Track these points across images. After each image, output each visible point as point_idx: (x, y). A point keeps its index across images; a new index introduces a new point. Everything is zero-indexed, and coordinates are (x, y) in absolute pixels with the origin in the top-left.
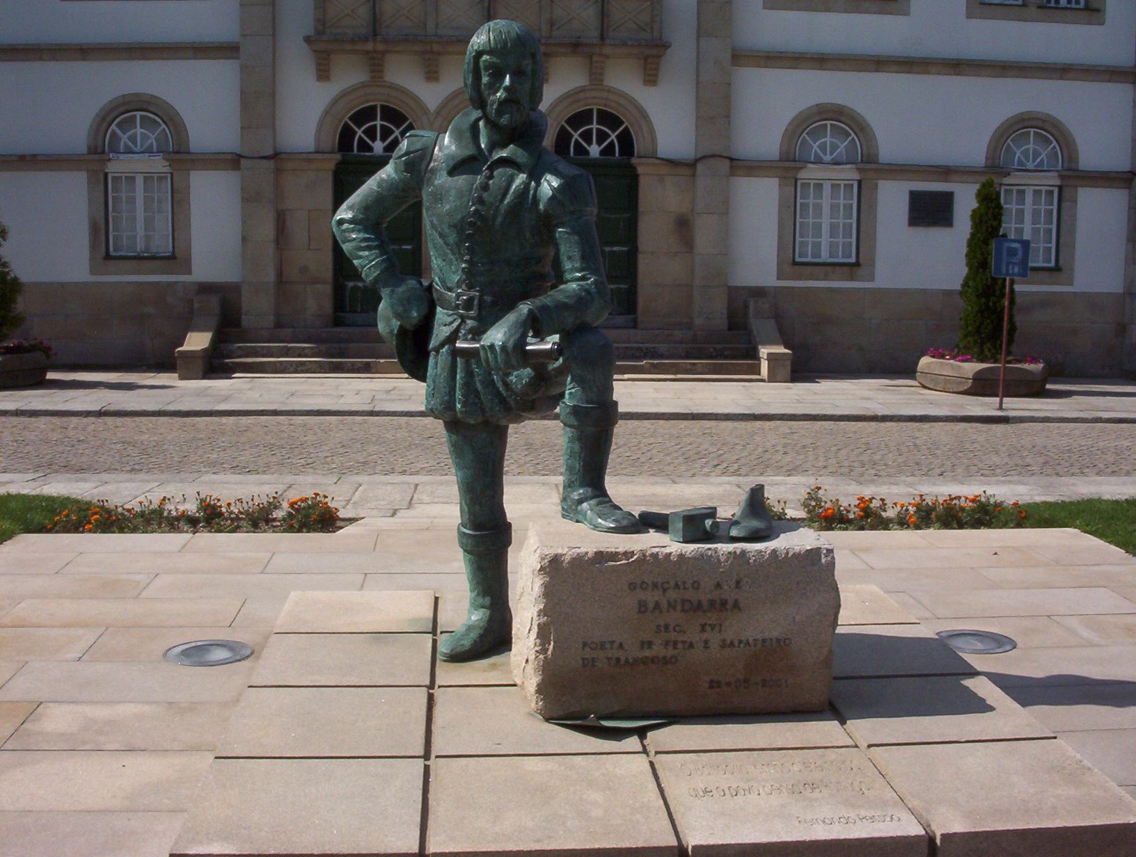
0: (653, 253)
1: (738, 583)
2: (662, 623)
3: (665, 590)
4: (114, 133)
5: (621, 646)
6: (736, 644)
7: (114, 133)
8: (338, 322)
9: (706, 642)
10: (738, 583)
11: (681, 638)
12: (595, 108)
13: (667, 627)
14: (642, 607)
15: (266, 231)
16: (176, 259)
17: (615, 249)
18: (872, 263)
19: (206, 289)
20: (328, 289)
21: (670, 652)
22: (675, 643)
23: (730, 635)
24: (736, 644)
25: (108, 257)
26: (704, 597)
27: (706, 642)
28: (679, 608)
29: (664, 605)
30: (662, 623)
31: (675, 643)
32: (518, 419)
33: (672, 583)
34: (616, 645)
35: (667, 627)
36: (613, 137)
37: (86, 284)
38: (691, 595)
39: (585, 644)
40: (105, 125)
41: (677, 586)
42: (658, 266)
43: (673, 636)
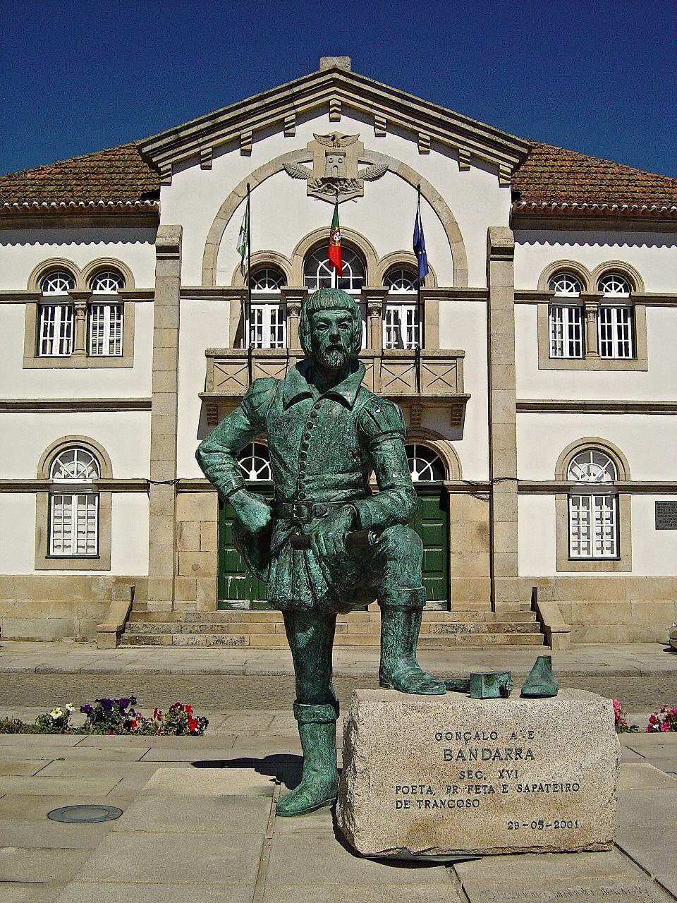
1: (531, 733)
2: (466, 769)
3: (467, 740)
4: (57, 462)
5: (430, 791)
6: (531, 789)
8: (220, 606)
9: (505, 786)
10: (531, 733)
11: (482, 783)
15: (168, 538)
16: (98, 559)
18: (629, 556)
19: (119, 580)
20: (213, 580)
21: (473, 796)
22: (477, 787)
24: (531, 789)
25: (48, 557)
26: (501, 745)
27: (505, 786)
28: (480, 755)
29: (467, 754)
30: (466, 769)
31: (477, 787)
32: (345, 610)
33: (473, 734)
35: (469, 772)
36: (429, 465)
37: (30, 578)
40: (50, 458)
41: (477, 736)
42: (466, 562)
43: (476, 782)
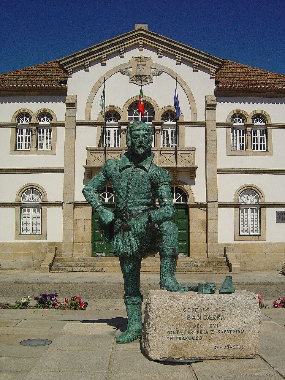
0: (194, 233)
2: (196, 324)
3: (197, 312)
4: (24, 194)
6: (224, 332)
7: (24, 194)
11: (203, 329)
12: (175, 187)
13: (198, 325)
14: (188, 318)
16: (41, 235)
17: (155, 34)
19: (50, 244)
21: (199, 335)
22: (201, 331)
23: (221, 329)
24: (224, 332)
26: (210, 314)
28: (202, 318)
29: (196, 317)
30: (196, 324)
31: (201, 331)
33: (199, 309)
34: (179, 332)
37: (13, 243)
38: (206, 313)
39: (168, 332)
41: (201, 310)
43: (200, 329)
